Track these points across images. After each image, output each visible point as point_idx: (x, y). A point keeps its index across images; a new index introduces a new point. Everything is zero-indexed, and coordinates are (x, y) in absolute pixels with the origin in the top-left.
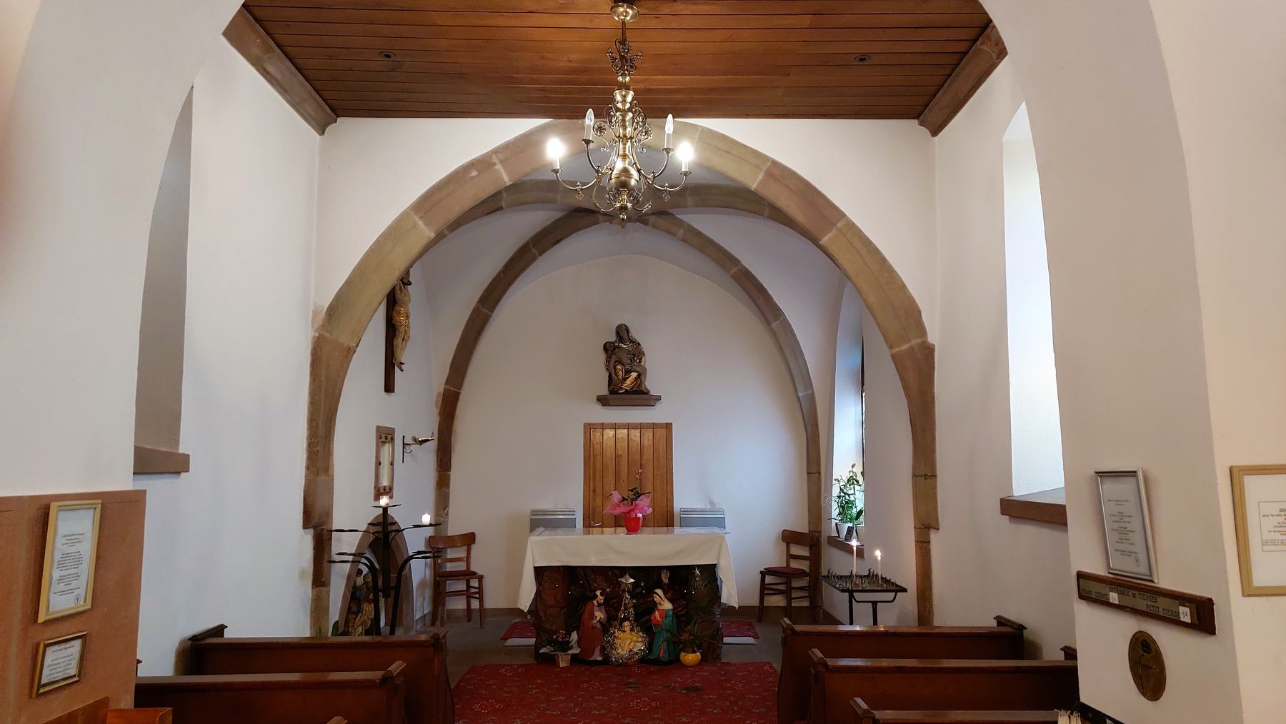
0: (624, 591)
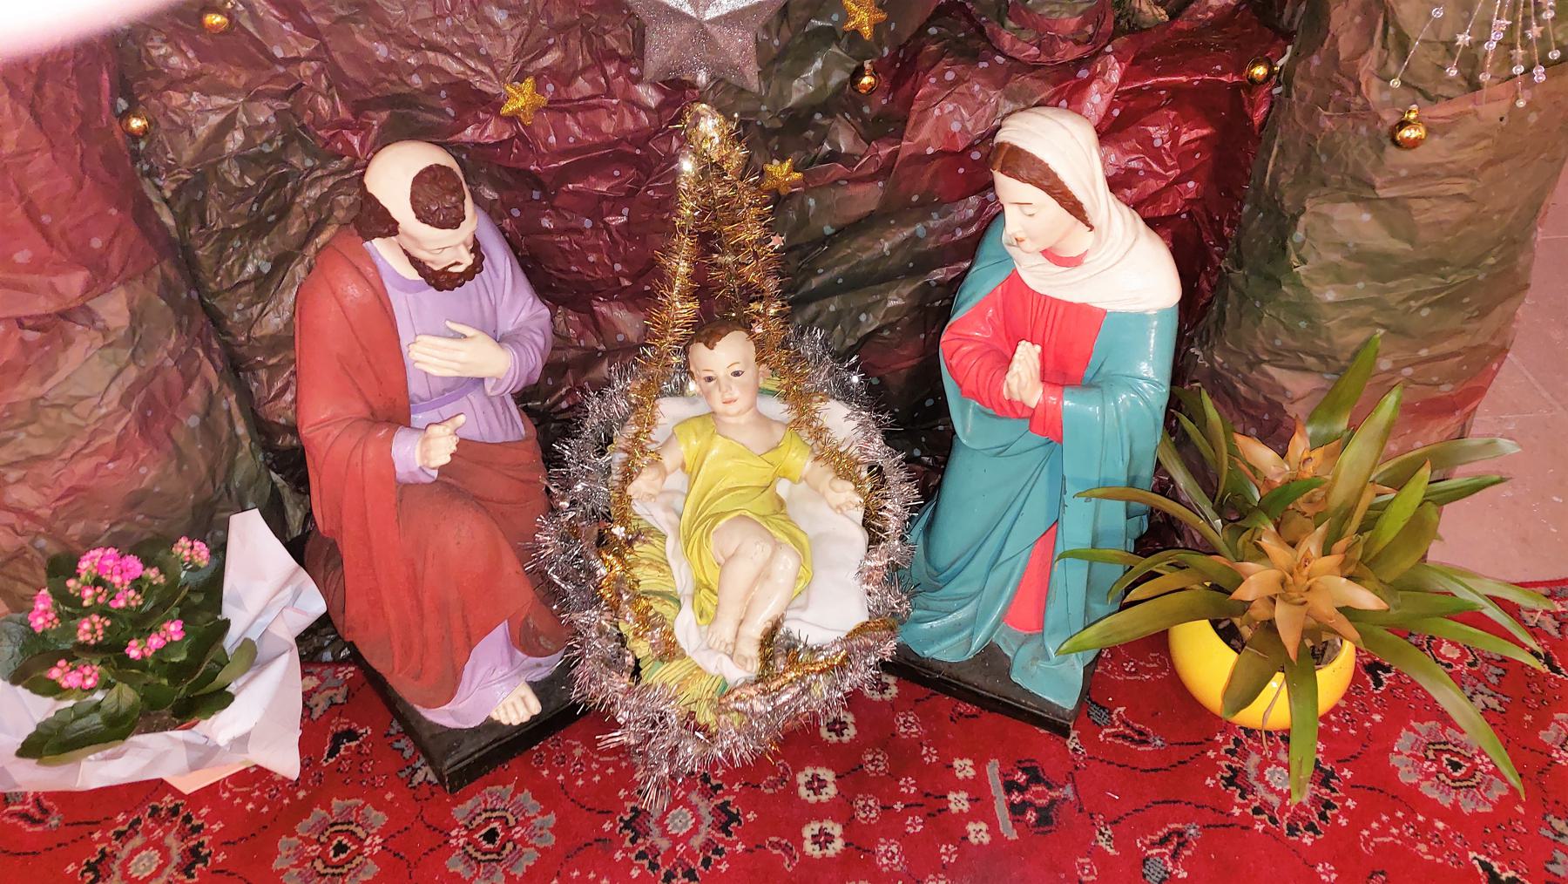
0: (678, 92)
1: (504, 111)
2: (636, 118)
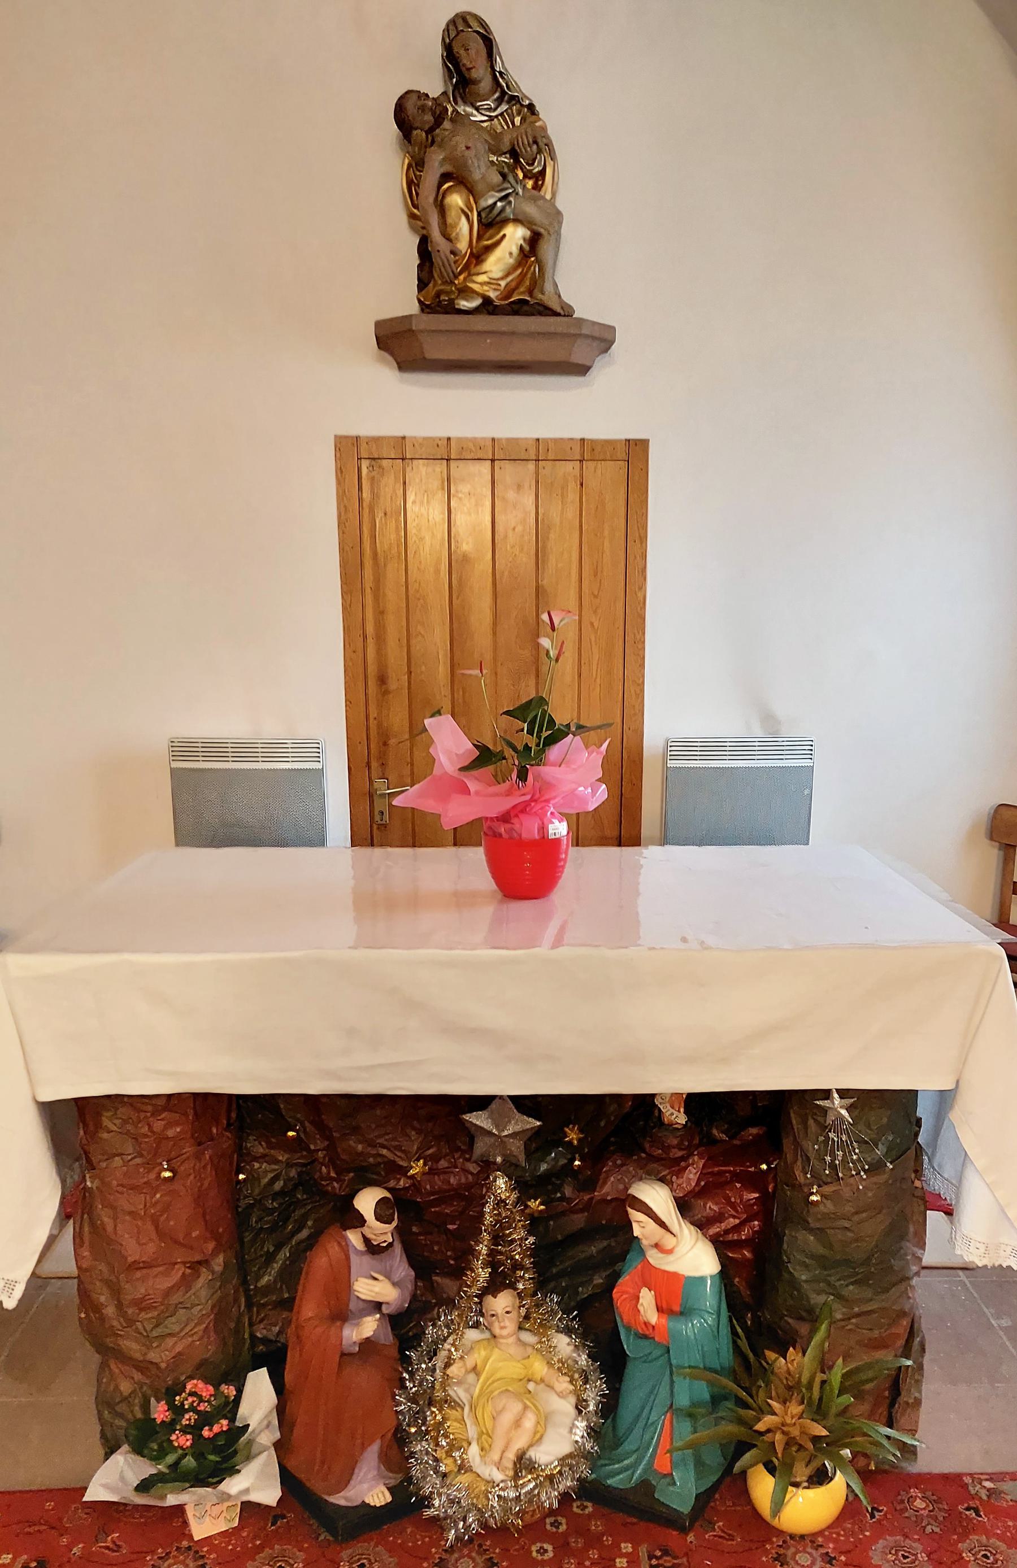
0: (487, 1166)
1: (409, 1174)
2: (467, 1178)
